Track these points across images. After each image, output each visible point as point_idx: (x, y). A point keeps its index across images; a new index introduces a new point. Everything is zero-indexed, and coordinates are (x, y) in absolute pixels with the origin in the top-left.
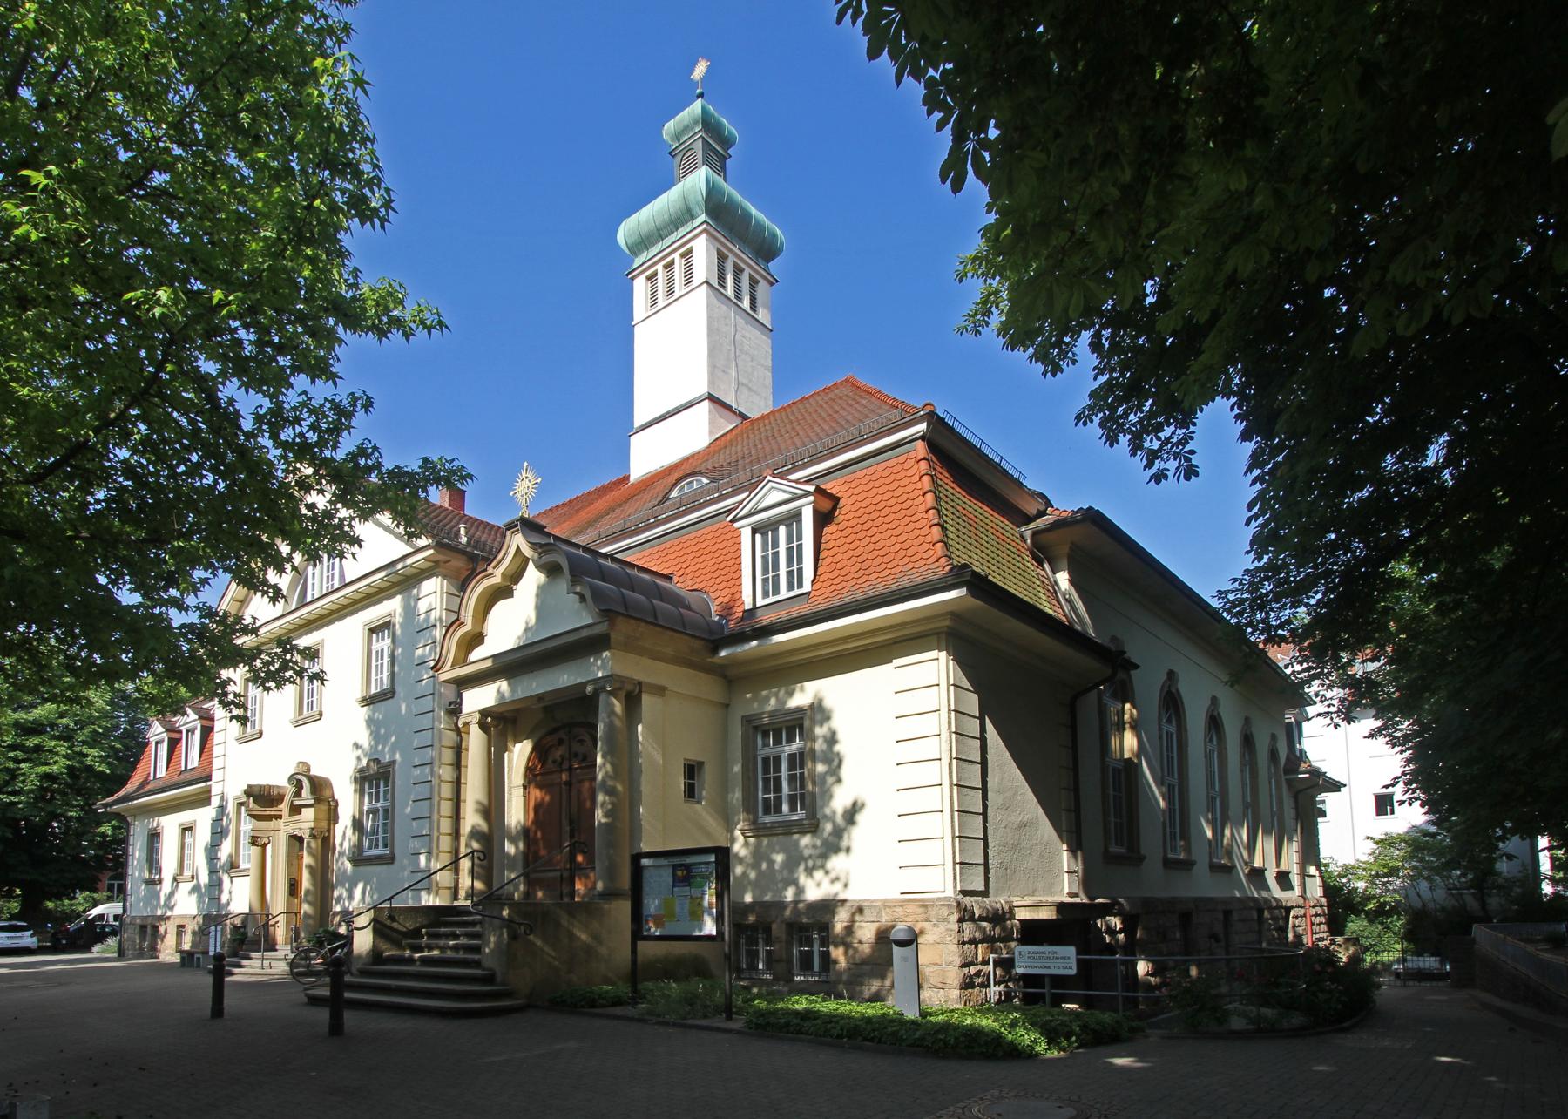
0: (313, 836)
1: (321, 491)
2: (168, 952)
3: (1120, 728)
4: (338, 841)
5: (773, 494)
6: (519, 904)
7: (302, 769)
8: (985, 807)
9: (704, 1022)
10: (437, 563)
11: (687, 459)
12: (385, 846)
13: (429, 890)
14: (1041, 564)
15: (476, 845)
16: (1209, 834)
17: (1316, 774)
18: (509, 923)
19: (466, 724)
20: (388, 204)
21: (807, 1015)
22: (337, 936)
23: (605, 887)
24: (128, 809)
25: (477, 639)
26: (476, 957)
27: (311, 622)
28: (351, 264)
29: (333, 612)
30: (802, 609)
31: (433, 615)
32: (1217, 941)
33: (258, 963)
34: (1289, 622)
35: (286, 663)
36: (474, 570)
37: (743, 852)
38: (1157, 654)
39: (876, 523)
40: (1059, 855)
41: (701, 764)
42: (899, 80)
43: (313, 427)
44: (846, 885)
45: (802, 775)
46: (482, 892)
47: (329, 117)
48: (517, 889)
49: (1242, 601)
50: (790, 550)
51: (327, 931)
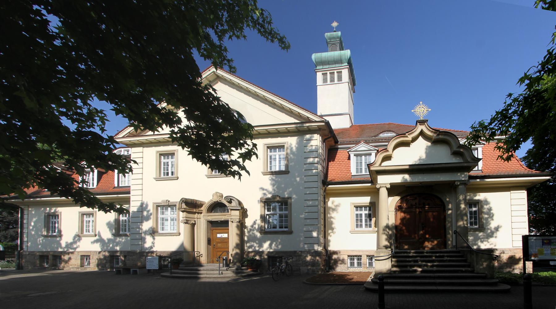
17: (111, 230)
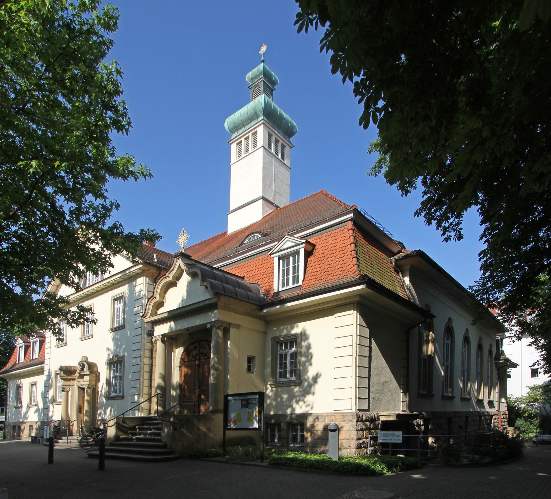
0: (89, 388)
1: (97, 243)
2: (25, 437)
3: (427, 342)
4: (100, 390)
5: (288, 243)
6: (176, 415)
7: (84, 359)
8: (370, 375)
9: (252, 463)
10: (144, 271)
11: (252, 225)
12: (120, 392)
13: (138, 410)
14: (398, 273)
15: (159, 392)
16: (461, 386)
17: (507, 360)
18: (173, 424)
19: (156, 340)
20: (129, 124)
21: (294, 460)
22: (99, 430)
23: (213, 409)
24: (7, 376)
25: (161, 304)
26: (159, 438)
27: (88, 296)
28: (111, 145)
29: (98, 291)
30: (298, 292)
31: (142, 293)
32: (462, 429)
33: (66, 441)
34: (497, 299)
35: (83, 317)
36: (160, 274)
37: (271, 394)
38: (445, 311)
39: (330, 256)
40: (399, 394)
41: (254, 357)
42: (344, 81)
43: (94, 216)
44: (312, 408)
45: (296, 362)
46: (161, 411)
47: (105, 87)
48: (176, 409)
49: (479, 290)
50: (294, 267)
51: (95, 428)
